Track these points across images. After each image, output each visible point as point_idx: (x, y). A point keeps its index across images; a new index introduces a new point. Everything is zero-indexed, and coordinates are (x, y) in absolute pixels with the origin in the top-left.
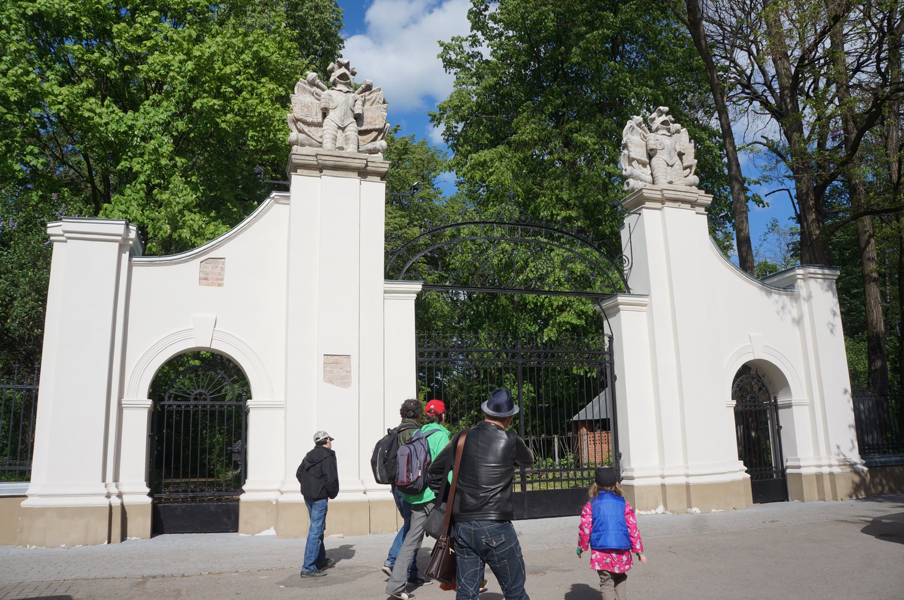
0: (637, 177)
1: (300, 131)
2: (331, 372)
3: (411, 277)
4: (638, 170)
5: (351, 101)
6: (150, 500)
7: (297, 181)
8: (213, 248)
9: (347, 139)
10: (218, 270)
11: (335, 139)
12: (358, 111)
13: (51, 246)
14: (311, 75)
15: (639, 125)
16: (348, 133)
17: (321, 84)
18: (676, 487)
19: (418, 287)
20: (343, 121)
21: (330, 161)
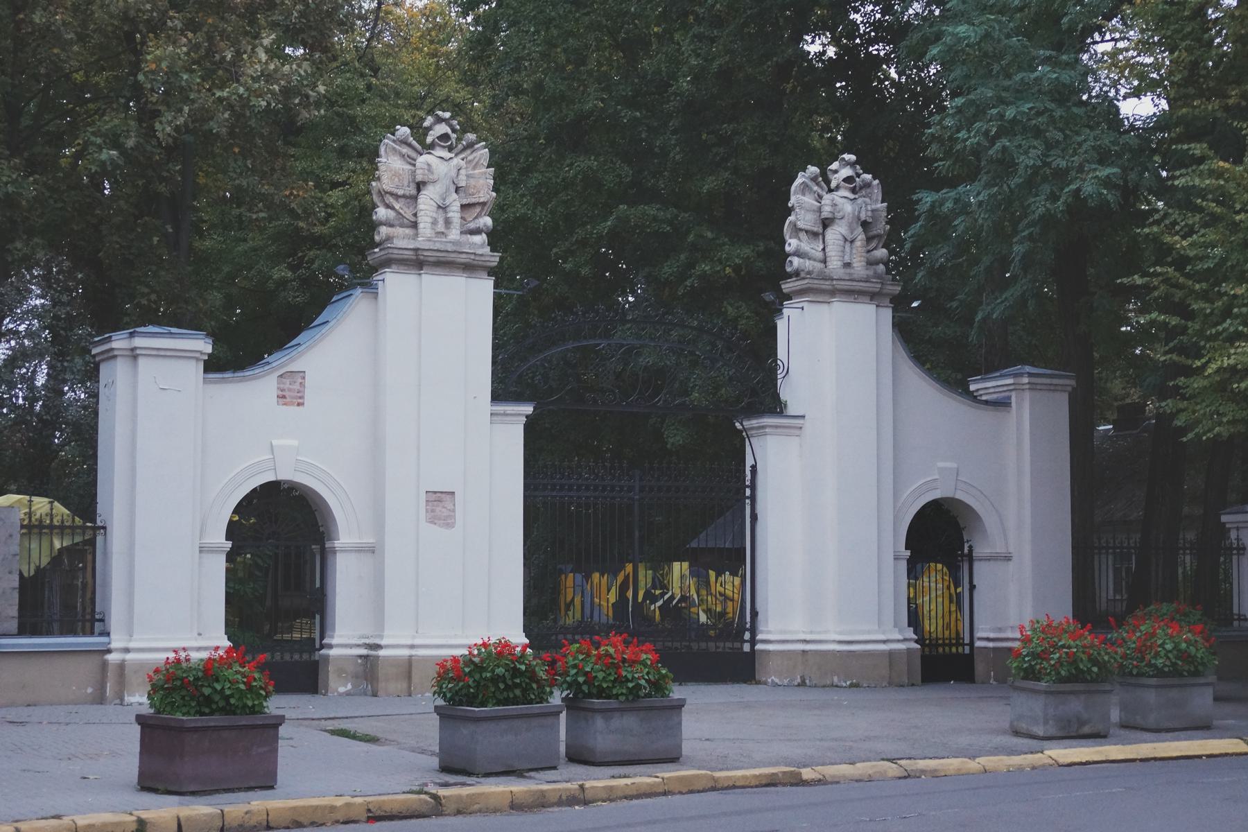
1: (388, 206)
2: (433, 511)
3: (518, 398)
4: (806, 245)
8: (292, 360)
10: (297, 386)
14: (403, 131)
15: (814, 179)
16: (450, 215)
18: (394, 661)
19: (529, 409)
20: (444, 200)
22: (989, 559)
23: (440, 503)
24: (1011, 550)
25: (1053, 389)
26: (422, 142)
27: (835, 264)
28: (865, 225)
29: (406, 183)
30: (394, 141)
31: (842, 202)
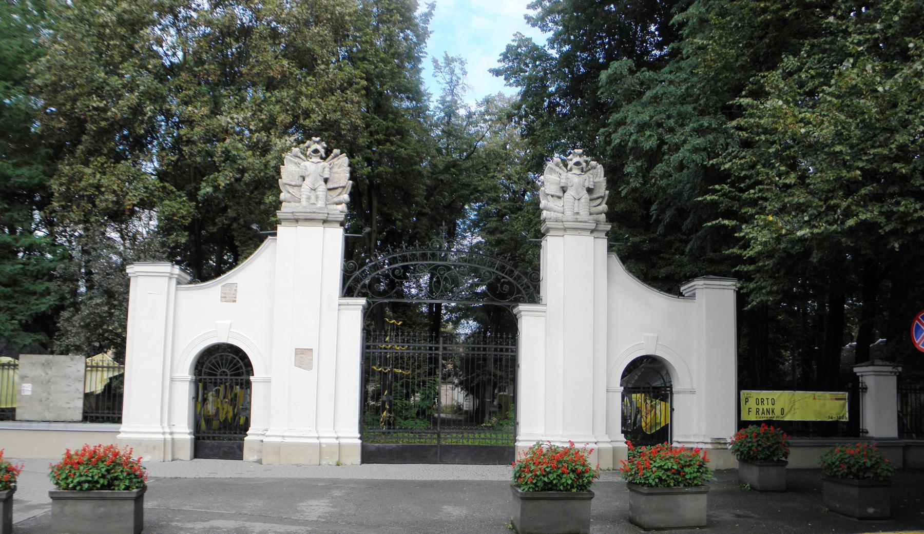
0: (552, 208)
5: (320, 170)
6: (360, 442)
7: (280, 229)
8: (230, 277)
9: (317, 197)
13: (129, 280)
17: (302, 156)
21: (302, 216)
22: (685, 392)
23: (303, 356)
24: (695, 387)
25: (724, 288)
27: (569, 214)
28: (590, 191)
31: (574, 178)
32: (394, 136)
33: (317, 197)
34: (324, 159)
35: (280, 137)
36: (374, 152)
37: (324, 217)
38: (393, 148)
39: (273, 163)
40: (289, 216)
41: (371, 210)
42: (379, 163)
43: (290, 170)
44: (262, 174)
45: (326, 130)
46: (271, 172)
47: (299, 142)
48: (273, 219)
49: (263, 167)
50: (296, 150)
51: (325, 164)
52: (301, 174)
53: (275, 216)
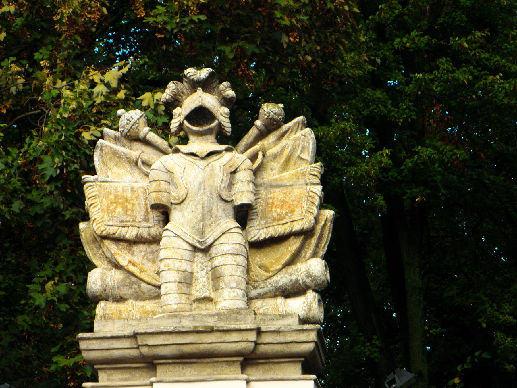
5: (219, 178)
9: (216, 276)
11: (187, 281)
12: (243, 195)
16: (216, 262)
17: (153, 137)
20: (202, 233)
26: (164, 130)
29: (140, 215)
30: (116, 139)
32: (464, 33)
33: (216, 276)
34: (230, 139)
35: (71, 76)
36: (395, 94)
37: (242, 342)
38: (463, 76)
39: (50, 166)
40: (123, 349)
41: (401, 306)
42: (418, 133)
43: (115, 187)
44: (17, 206)
45: (229, 36)
46: (45, 198)
47: (136, 85)
48: (63, 361)
49: (16, 182)
50: (130, 117)
51: (238, 158)
52: (153, 199)
53: (73, 349)
